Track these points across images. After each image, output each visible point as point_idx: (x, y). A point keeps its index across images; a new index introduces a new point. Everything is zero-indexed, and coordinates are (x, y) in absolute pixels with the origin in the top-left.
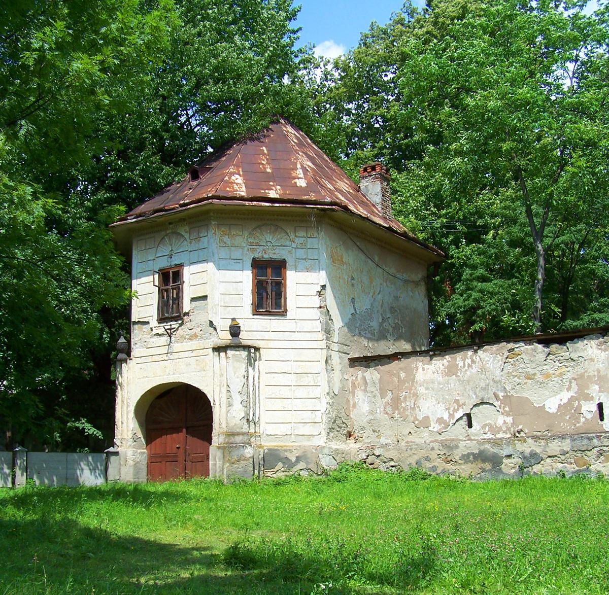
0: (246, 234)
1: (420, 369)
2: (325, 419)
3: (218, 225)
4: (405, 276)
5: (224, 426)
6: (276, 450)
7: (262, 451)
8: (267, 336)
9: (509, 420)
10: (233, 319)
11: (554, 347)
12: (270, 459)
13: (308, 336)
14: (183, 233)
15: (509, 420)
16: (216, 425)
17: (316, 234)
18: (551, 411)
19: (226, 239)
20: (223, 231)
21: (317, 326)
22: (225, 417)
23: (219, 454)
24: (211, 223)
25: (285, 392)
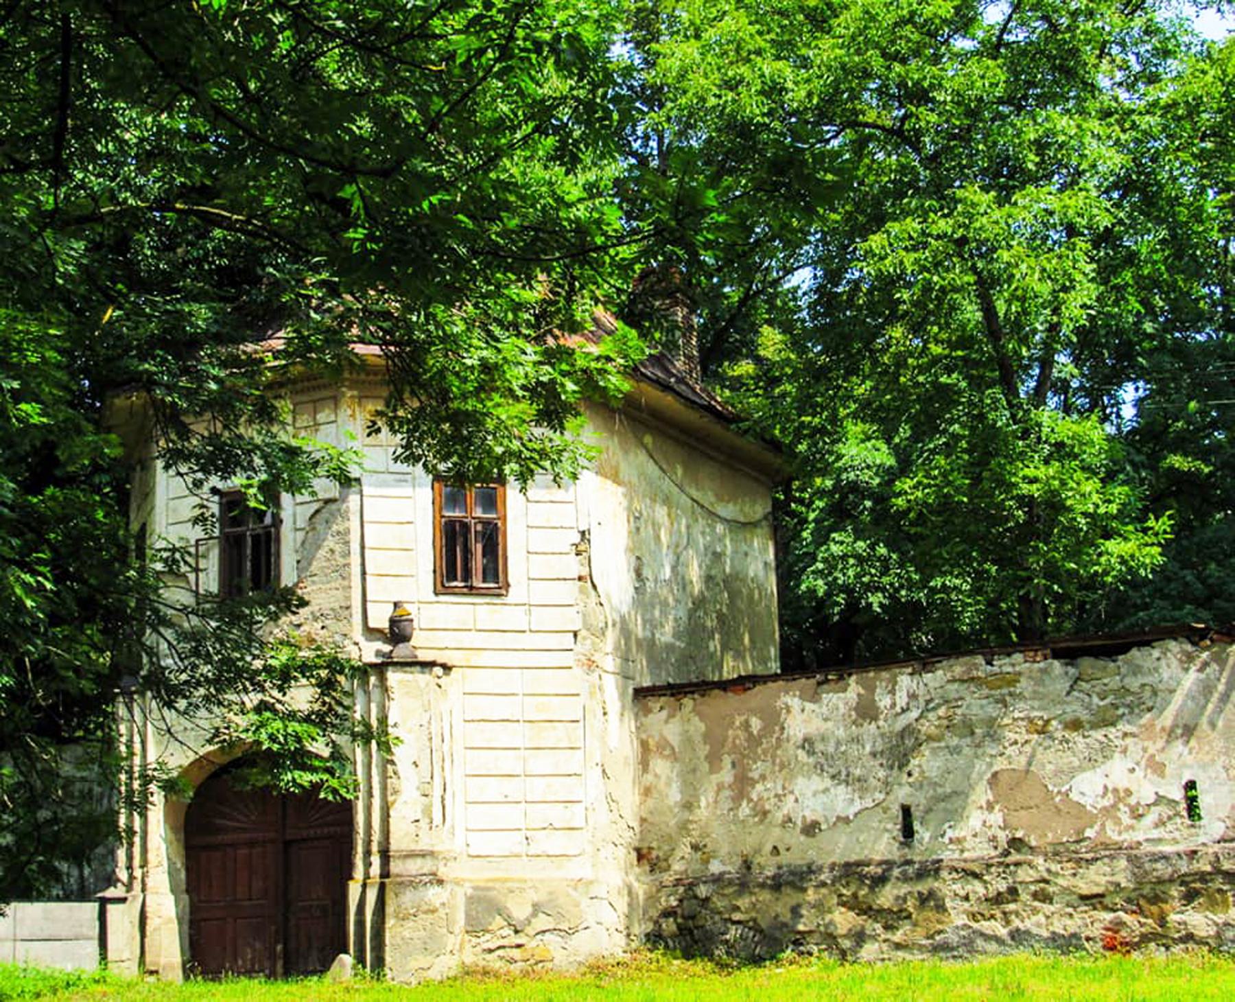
3: (360, 398)
4: (728, 510)
6: (488, 889)
11: (1086, 663)
24: (343, 394)
25: (508, 762)
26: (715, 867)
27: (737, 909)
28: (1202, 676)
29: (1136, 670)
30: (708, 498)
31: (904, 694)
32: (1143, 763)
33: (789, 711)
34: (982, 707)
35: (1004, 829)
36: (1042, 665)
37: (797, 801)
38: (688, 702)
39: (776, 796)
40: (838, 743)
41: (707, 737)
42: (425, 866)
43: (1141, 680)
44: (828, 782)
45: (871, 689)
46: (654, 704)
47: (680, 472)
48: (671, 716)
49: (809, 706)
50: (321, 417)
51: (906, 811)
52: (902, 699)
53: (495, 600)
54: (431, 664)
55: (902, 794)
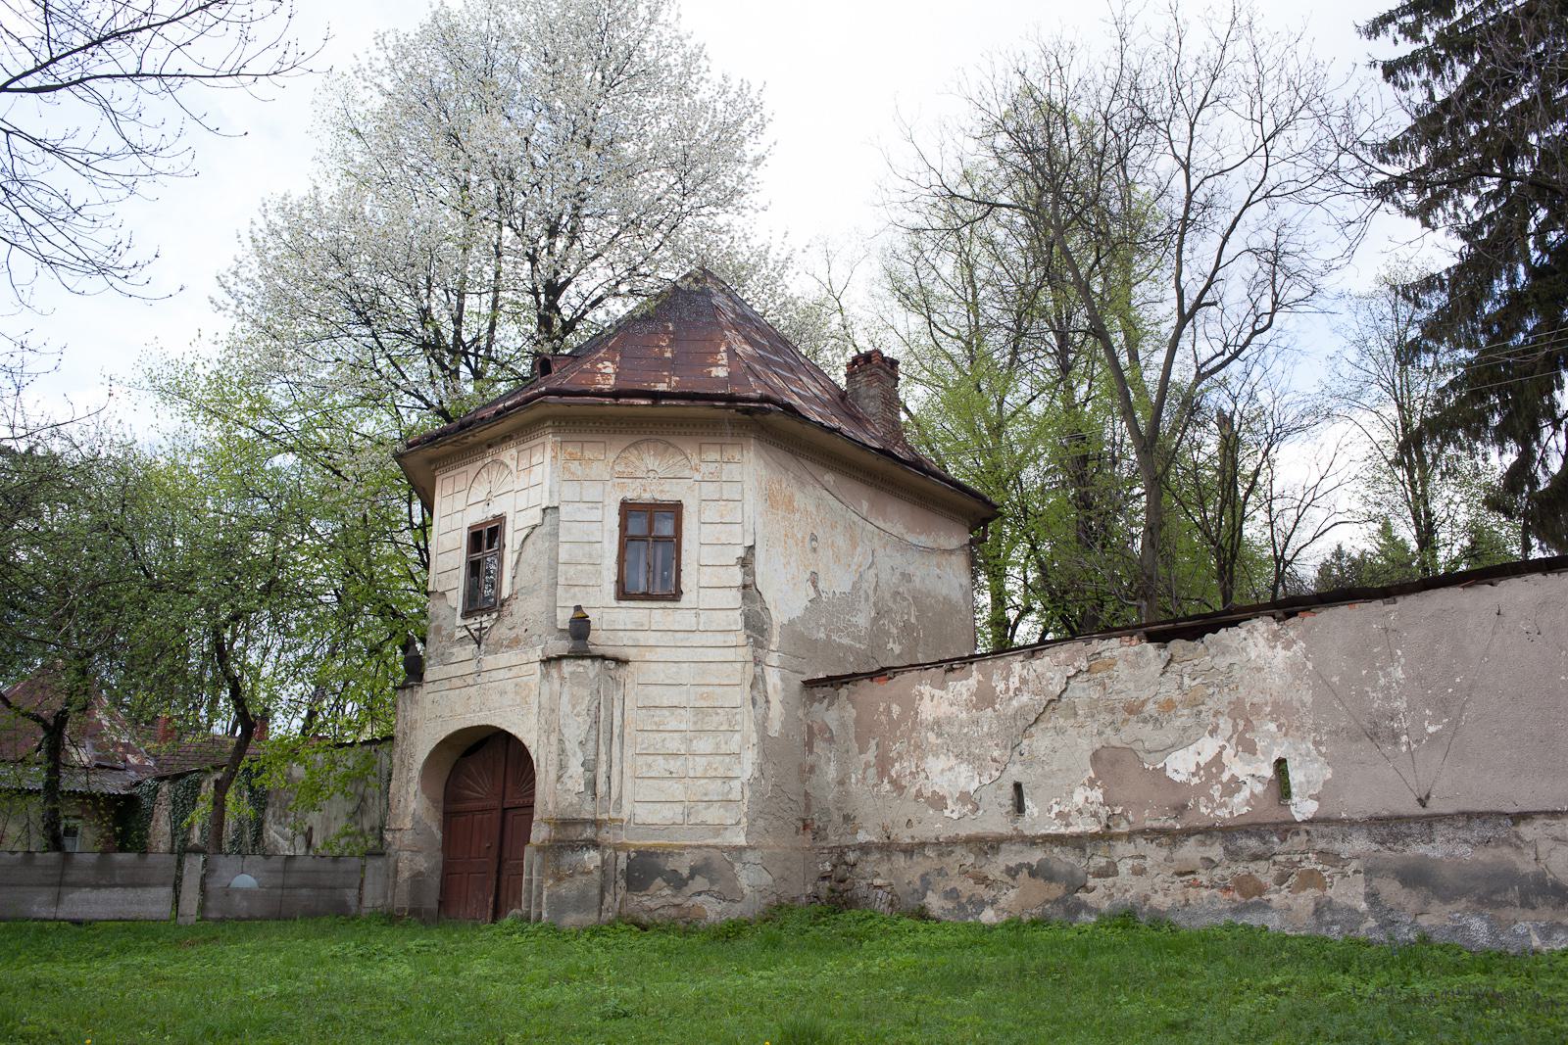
0: (612, 456)
1: (927, 697)
2: (747, 794)
4: (924, 540)
5: (550, 807)
7: (623, 856)
8: (652, 639)
9: (1097, 795)
10: (578, 608)
11: (1177, 645)
12: (643, 868)
13: (719, 639)
14: (507, 461)
15: (1097, 795)
16: (538, 807)
17: (738, 457)
18: (1177, 778)
19: (574, 466)
20: (570, 454)
21: (737, 620)
22: (556, 789)
23: (537, 860)
26: (862, 837)
27: (878, 875)
28: (1289, 654)
29: (1224, 651)
30: (898, 529)
31: (1017, 680)
32: (1233, 741)
33: (922, 698)
34: (1084, 689)
35: (1103, 805)
36: (1136, 648)
37: (927, 778)
38: (843, 691)
39: (911, 773)
40: (961, 726)
41: (857, 721)
42: (589, 833)
43: (1229, 660)
44: (953, 761)
45: (988, 676)
46: (818, 692)
47: (865, 505)
48: (831, 704)
49: (937, 693)
50: (534, 460)
51: (1018, 787)
52: (1014, 682)
53: (669, 605)
54: (604, 658)
55: (1015, 772)
